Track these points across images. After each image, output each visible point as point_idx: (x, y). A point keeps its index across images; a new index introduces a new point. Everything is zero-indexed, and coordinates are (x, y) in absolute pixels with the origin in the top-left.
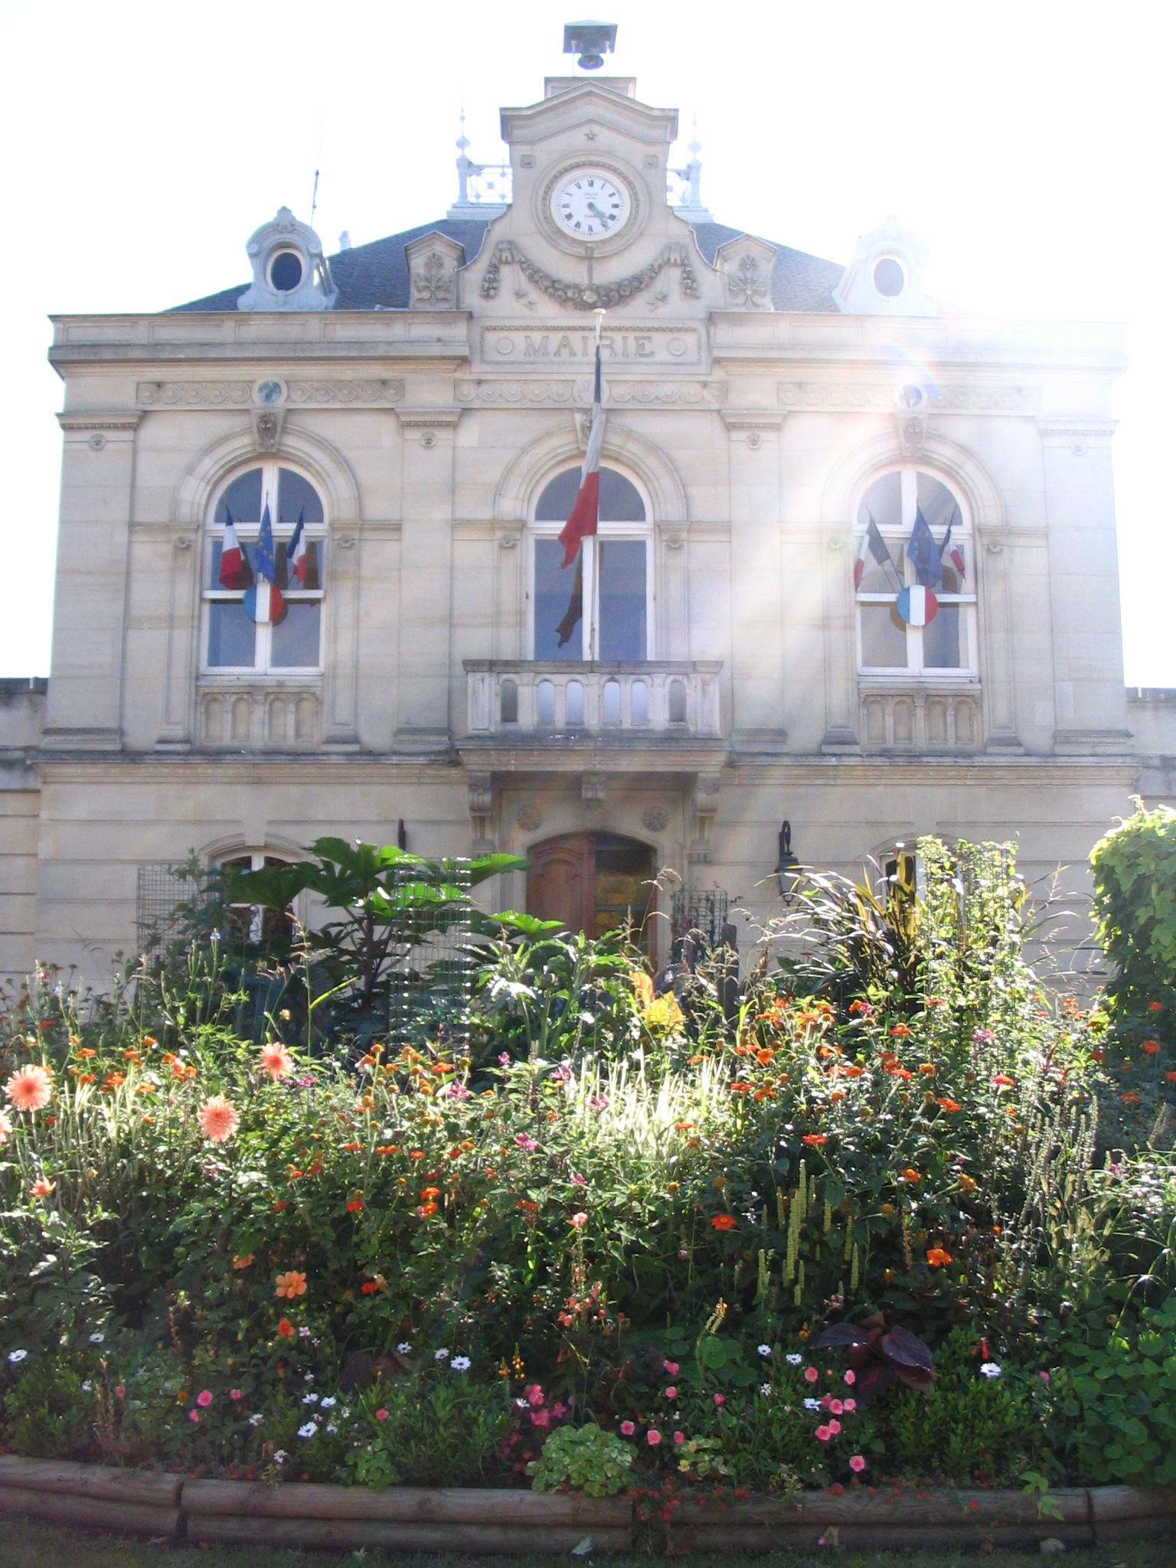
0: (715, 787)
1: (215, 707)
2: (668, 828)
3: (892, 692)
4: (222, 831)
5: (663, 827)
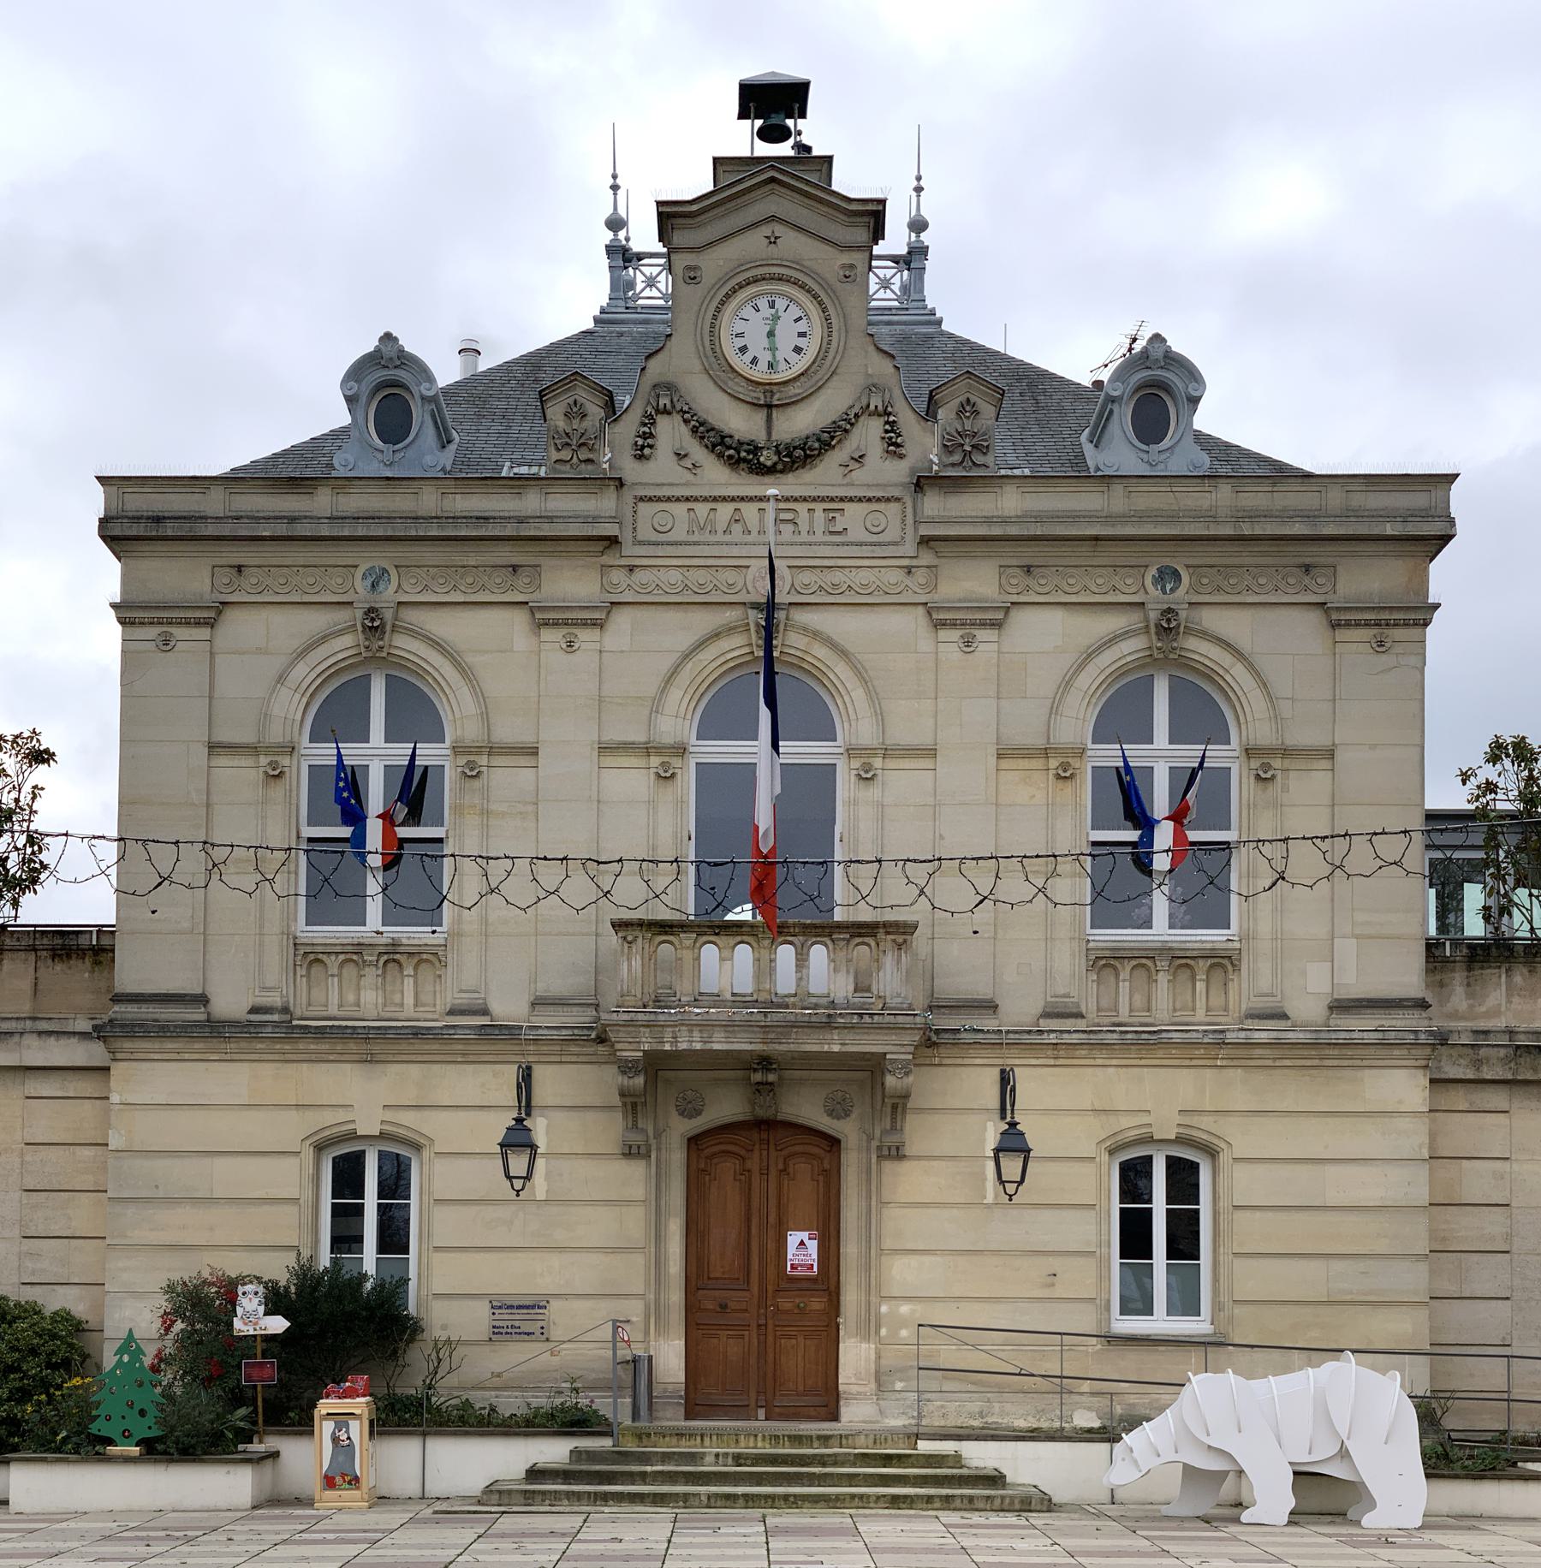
1: (316, 969)
2: (853, 1116)
4: (329, 1118)
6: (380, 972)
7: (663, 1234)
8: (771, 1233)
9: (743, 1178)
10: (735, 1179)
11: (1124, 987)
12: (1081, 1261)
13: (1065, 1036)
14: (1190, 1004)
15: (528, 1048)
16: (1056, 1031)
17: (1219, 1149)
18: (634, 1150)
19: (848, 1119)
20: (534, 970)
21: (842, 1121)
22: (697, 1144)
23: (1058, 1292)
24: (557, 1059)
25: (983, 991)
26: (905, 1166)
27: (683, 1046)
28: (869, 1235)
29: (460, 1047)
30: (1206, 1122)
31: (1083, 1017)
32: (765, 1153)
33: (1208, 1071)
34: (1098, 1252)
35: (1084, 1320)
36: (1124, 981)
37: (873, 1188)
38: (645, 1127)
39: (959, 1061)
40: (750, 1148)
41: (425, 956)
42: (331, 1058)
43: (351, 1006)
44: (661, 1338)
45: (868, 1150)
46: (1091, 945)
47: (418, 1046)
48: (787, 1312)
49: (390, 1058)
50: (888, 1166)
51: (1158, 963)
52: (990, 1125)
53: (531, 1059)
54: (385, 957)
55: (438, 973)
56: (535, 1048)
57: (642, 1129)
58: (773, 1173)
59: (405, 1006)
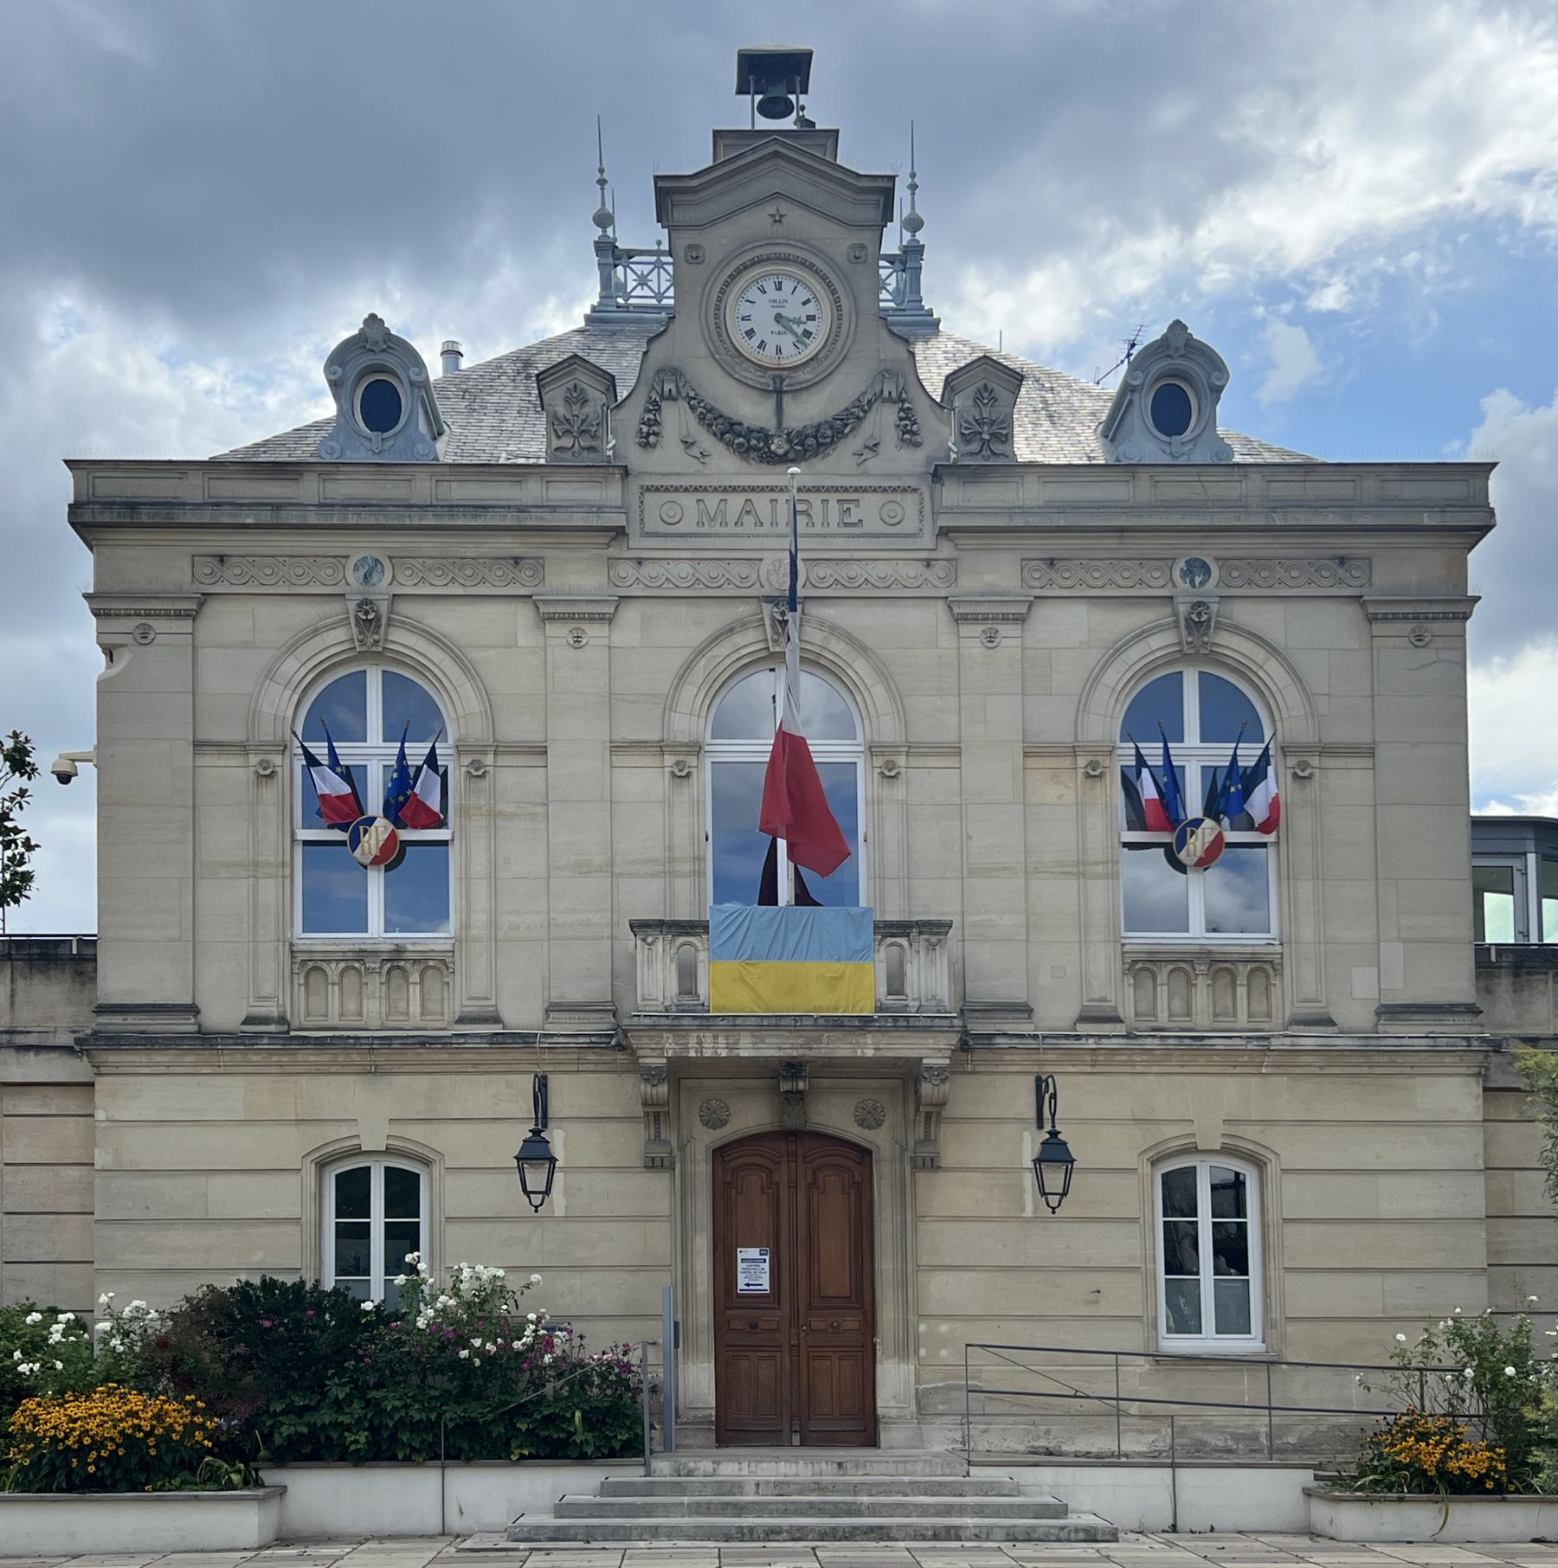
0: (942, 1074)
1: (315, 978)
2: (886, 1124)
4: (331, 1133)
5: (879, 1124)
6: (384, 979)
10: (762, 1193)
11: (1163, 991)
13: (1104, 1041)
15: (543, 1057)
17: (1266, 1160)
18: (658, 1163)
19: (880, 1129)
20: (547, 976)
23: (1105, 1309)
24: (574, 1068)
25: (1018, 995)
26: (942, 1176)
27: (708, 1053)
28: (902, 1255)
29: (471, 1056)
30: (1251, 1132)
31: (1121, 1021)
32: (793, 1165)
33: (1254, 1080)
34: (1143, 1266)
35: (1131, 1338)
36: (1162, 985)
41: (431, 963)
42: (333, 1069)
43: (353, 1015)
46: (1126, 948)
47: (425, 1055)
48: (820, 1331)
49: (396, 1069)
50: (922, 1177)
52: (1026, 1134)
53: (547, 1068)
54: (389, 965)
55: (446, 980)
56: (551, 1056)
57: (665, 1140)
58: (802, 1185)
59: (411, 1015)
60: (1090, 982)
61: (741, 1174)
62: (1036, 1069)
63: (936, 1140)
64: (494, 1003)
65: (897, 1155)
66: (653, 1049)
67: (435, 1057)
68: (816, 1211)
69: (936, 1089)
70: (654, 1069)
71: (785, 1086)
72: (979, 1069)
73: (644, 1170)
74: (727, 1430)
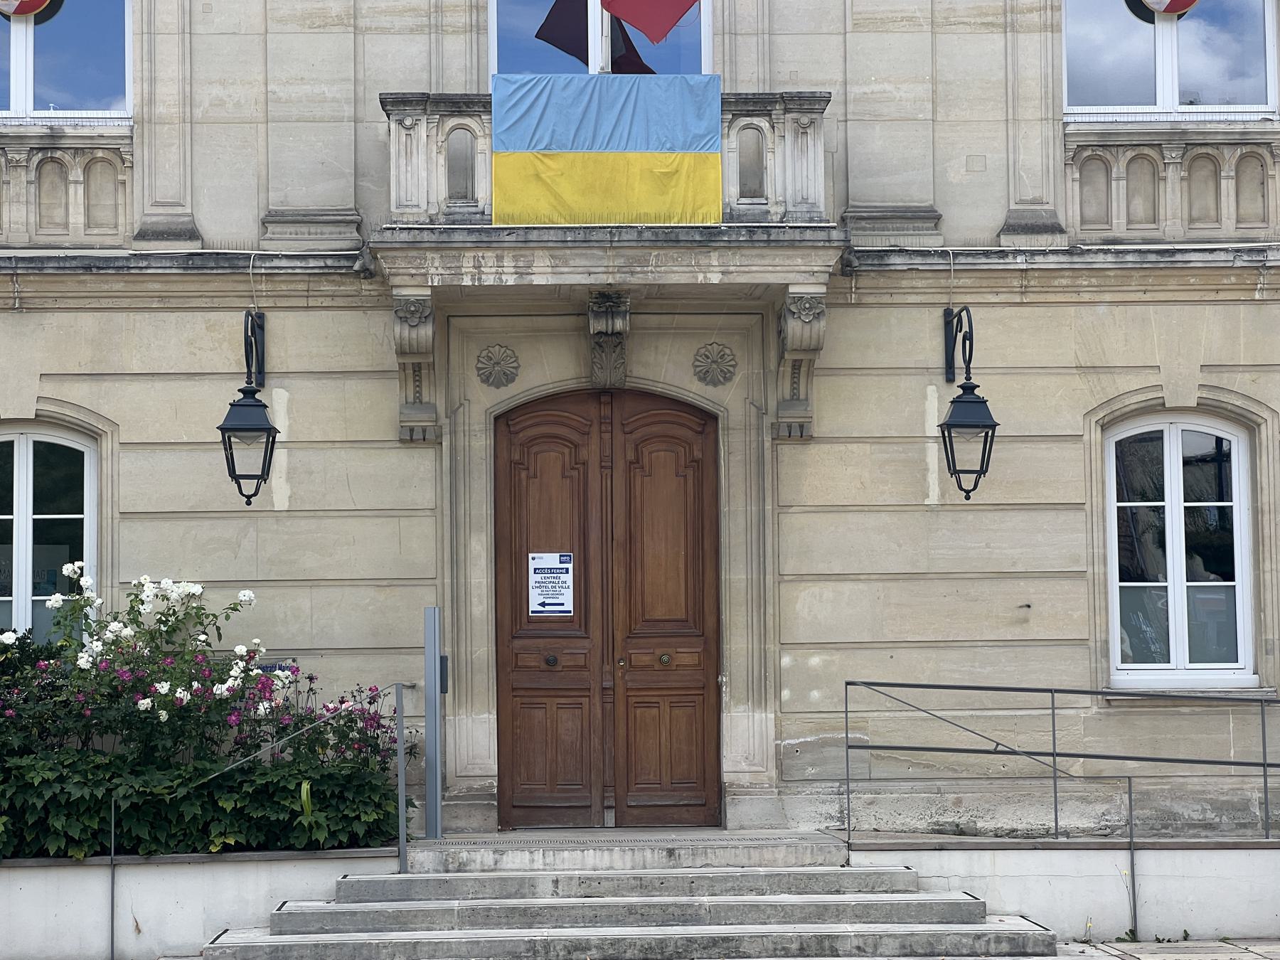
0: (815, 307)
2: (737, 379)
3: (1123, 140)
5: (727, 377)
7: (462, 556)
8: (619, 555)
9: (575, 473)
10: (564, 476)
12: (1066, 585)
13: (1039, 259)
14: (1213, 213)
15: (259, 287)
16: (1024, 252)
17: (1260, 420)
19: (729, 385)
21: (720, 387)
22: (508, 425)
24: (303, 302)
25: (919, 196)
26: (814, 450)
27: (489, 280)
29: (157, 286)
30: (1240, 382)
32: (607, 436)
34: (1090, 570)
37: (768, 485)
38: (432, 401)
39: (886, 299)
40: (586, 429)
41: (100, 154)
44: (463, 710)
45: (759, 429)
46: (1071, 129)
47: (91, 283)
48: (644, 668)
50: (787, 450)
51: (1166, 153)
53: (263, 303)
55: (120, 177)
56: (270, 287)
57: (428, 403)
58: (620, 466)
60: (1021, 177)
61: (535, 449)
62: (945, 299)
63: (807, 399)
64: (189, 211)
65: (754, 420)
66: (412, 275)
67: (106, 287)
68: (638, 500)
69: (807, 327)
70: (413, 303)
71: (597, 326)
72: (870, 299)
73: (398, 445)
74: (514, 807)
